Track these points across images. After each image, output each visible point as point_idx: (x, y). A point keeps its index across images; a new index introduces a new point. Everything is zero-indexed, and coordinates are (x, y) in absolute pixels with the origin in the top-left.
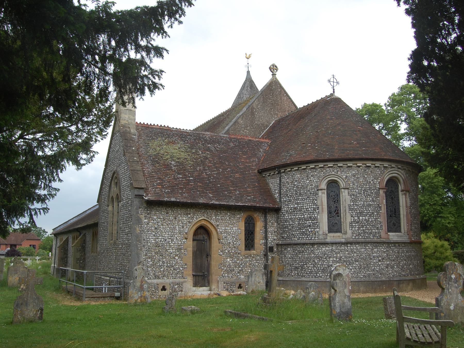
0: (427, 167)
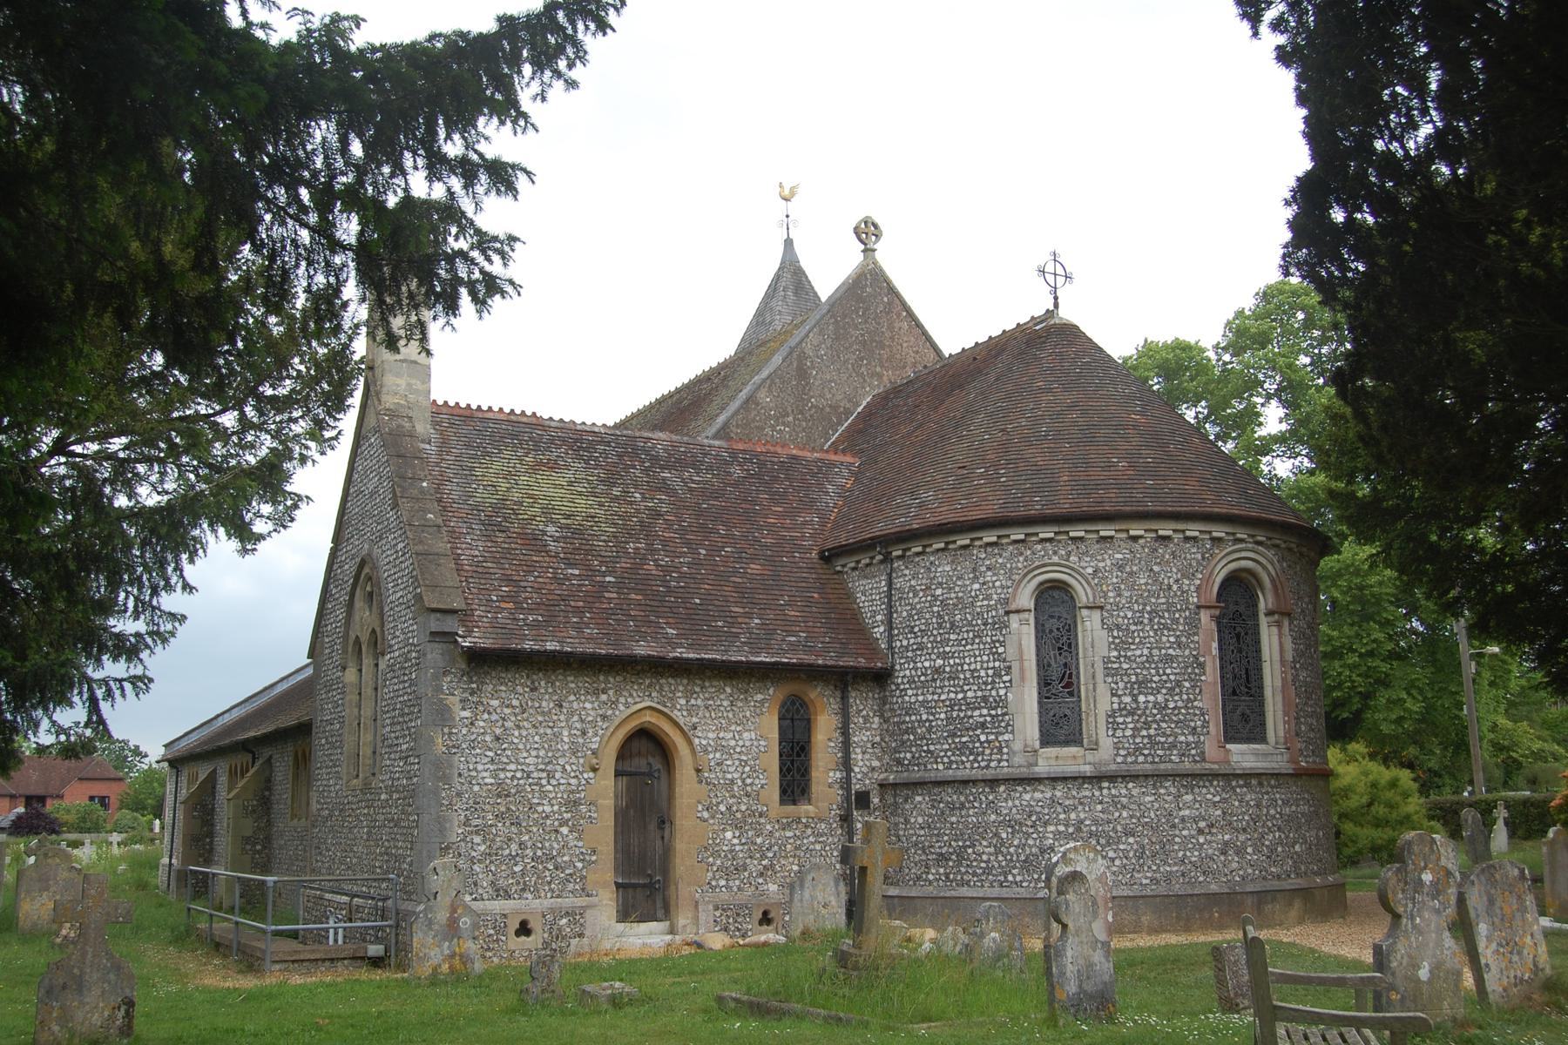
0: (1344, 537)
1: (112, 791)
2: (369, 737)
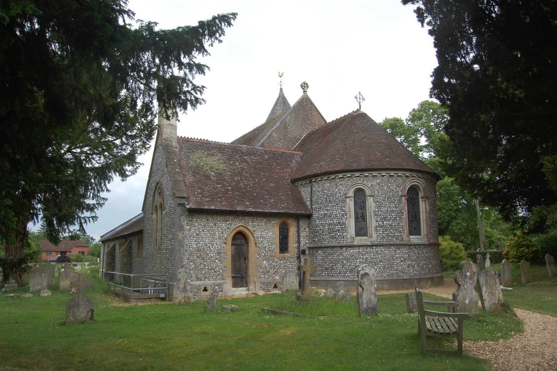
0: (444, 176)
1: (86, 250)
2: (160, 234)
